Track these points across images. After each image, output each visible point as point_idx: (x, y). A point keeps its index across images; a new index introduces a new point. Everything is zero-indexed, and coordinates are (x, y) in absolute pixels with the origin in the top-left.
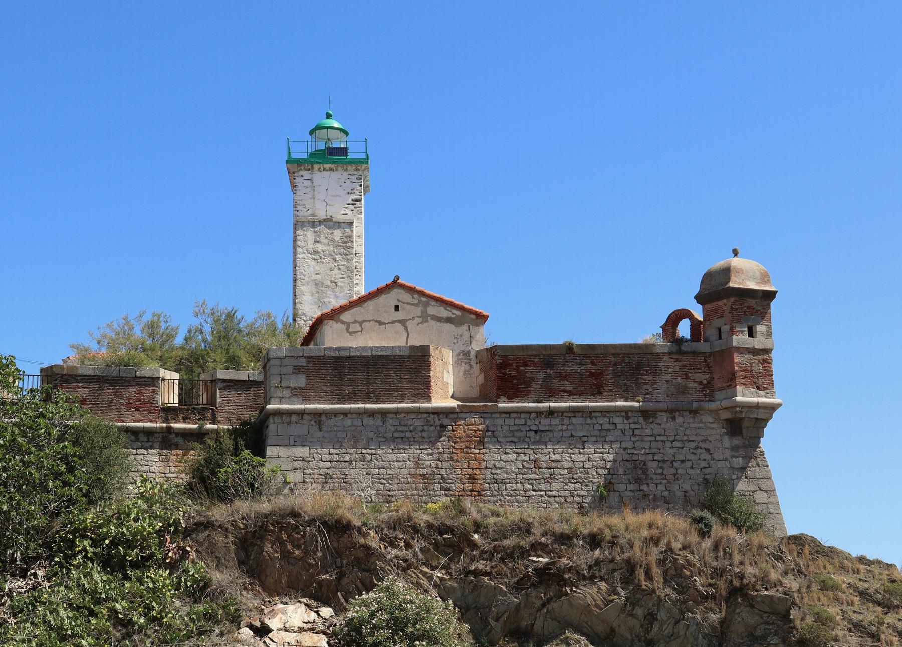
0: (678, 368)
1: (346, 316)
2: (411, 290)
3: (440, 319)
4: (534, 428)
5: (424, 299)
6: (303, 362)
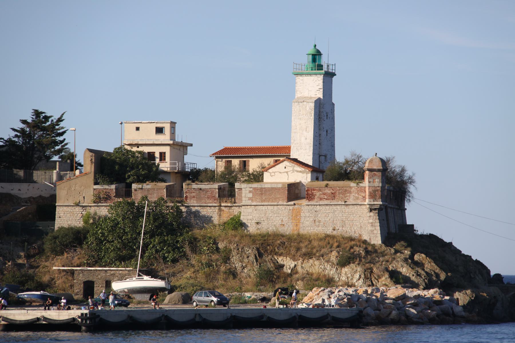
1: (270, 170)
3: (297, 171)
6: (251, 189)
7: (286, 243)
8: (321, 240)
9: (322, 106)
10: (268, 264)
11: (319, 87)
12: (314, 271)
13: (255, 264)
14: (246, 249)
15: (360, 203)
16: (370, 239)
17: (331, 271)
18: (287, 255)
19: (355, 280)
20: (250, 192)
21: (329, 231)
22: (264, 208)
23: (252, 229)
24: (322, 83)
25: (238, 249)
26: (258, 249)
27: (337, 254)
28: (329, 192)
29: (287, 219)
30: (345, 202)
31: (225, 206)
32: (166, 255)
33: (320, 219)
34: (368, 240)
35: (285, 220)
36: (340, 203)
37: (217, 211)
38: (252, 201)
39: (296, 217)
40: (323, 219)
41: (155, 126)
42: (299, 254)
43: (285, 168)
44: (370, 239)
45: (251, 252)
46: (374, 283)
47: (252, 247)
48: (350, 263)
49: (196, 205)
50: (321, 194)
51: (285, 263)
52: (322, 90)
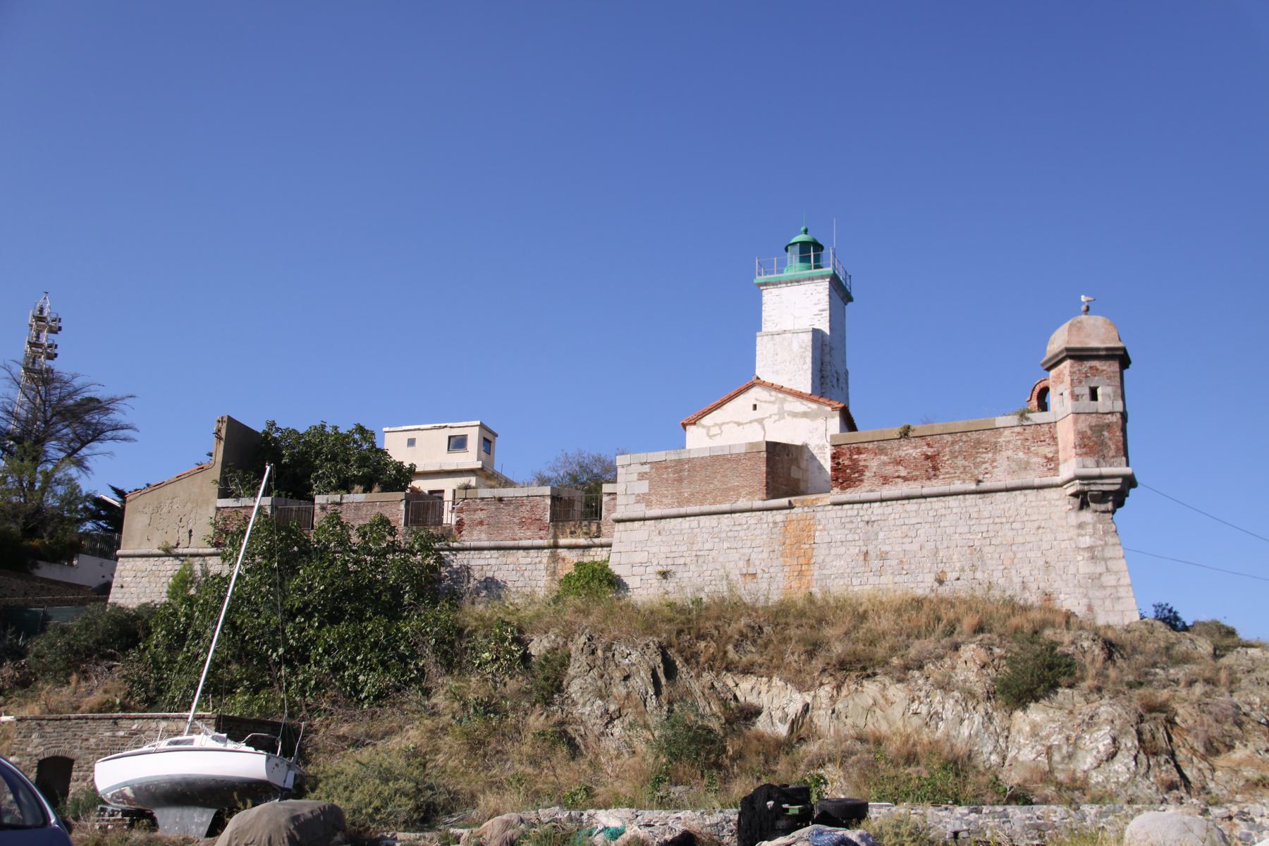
0: (1019, 442)
1: (707, 420)
2: (772, 387)
4: (866, 518)
5: (781, 395)
6: (646, 468)
7: (767, 629)
8: (899, 611)
9: (827, 349)
10: (702, 703)
11: (821, 307)
12: (884, 728)
13: (652, 702)
14: (620, 648)
15: (1037, 482)
16: (1090, 608)
17: (962, 726)
18: (769, 669)
19: (1086, 762)
20: (642, 476)
21: (923, 586)
22: (685, 523)
23: (644, 590)
24: (827, 298)
25: (593, 652)
26: (663, 650)
27: (982, 654)
28: (915, 453)
29: (765, 555)
30: (979, 482)
31: (570, 547)
32: (361, 678)
33: (886, 548)
34: (1079, 609)
35: (760, 559)
36: (958, 486)
37: (545, 560)
38: (649, 504)
39: (798, 547)
40: (898, 548)
41: (447, 433)
42: (818, 663)
43: (755, 407)
44: (1090, 608)
45: (637, 660)
46: (1190, 773)
47: (641, 642)
48: (1054, 686)
49: (486, 544)
50: (885, 464)
51: (764, 700)
52: (827, 314)
